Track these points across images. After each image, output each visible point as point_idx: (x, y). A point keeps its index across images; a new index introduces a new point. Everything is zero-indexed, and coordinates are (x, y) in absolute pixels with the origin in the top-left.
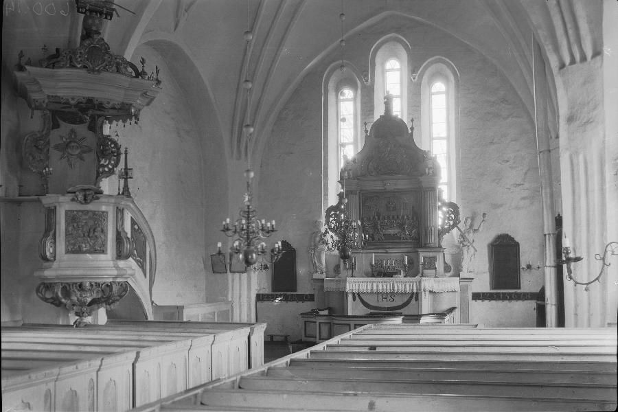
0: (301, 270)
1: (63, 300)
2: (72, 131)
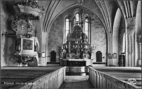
0: (57, 57)
1: (22, 61)
2: (22, 21)
